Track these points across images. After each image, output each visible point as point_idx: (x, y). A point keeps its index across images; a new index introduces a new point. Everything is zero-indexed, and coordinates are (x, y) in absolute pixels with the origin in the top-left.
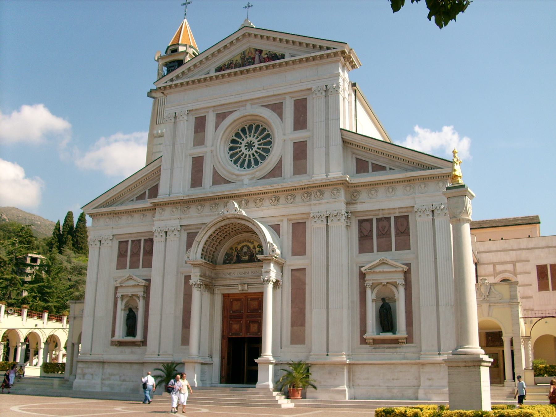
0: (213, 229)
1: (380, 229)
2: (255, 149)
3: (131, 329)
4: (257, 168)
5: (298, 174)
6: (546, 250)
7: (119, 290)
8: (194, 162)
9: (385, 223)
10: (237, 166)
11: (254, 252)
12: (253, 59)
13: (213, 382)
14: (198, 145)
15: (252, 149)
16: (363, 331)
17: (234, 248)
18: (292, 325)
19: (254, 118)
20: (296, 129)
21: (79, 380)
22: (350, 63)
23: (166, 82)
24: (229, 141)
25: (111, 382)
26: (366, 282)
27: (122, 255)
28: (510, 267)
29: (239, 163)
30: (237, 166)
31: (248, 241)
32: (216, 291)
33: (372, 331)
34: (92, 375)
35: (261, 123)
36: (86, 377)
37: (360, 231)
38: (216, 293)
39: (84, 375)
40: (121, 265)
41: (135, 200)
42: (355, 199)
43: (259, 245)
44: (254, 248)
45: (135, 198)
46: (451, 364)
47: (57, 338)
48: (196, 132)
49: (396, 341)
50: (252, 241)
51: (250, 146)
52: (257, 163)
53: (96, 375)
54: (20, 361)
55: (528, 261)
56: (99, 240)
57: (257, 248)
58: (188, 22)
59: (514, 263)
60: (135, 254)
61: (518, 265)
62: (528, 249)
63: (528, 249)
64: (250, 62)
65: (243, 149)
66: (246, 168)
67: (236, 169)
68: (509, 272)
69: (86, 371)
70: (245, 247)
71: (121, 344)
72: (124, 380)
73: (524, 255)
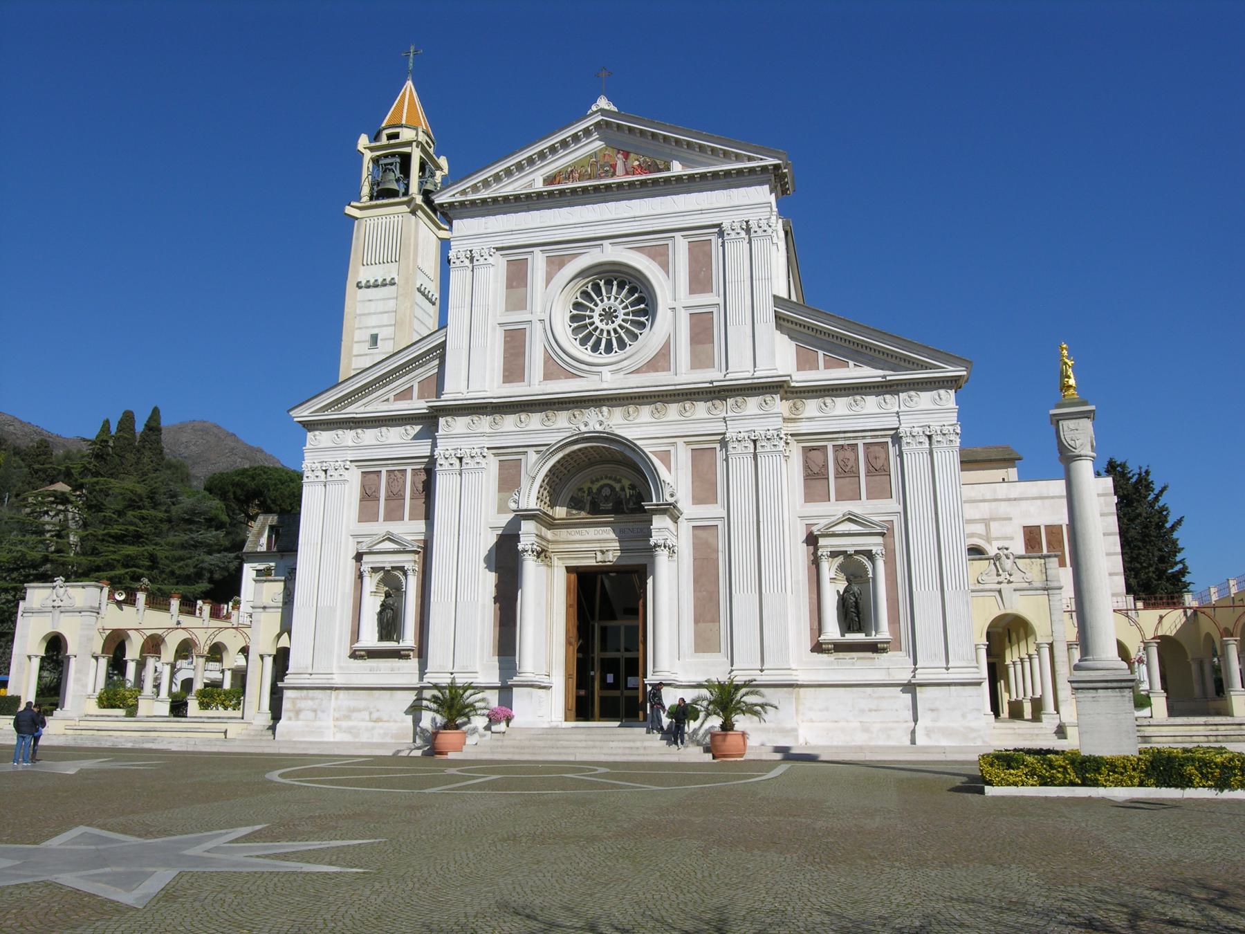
0: (560, 455)
1: (841, 463)
2: (619, 321)
3: (389, 624)
4: (621, 354)
5: (699, 368)
6: (1039, 502)
7: (365, 558)
8: (508, 339)
9: (849, 454)
10: (586, 349)
11: (623, 497)
12: (614, 166)
13: (553, 719)
14: (514, 310)
15: (607, 324)
16: (819, 627)
17: (585, 489)
18: (696, 621)
19: (616, 268)
20: (692, 291)
21: (289, 722)
22: (781, 185)
23: (454, 195)
24: (571, 307)
25: (351, 723)
26: (820, 550)
27: (368, 496)
28: (979, 529)
29: (590, 343)
30: (586, 349)
31: (610, 478)
32: (556, 562)
33: (370, 637)
34: (315, 711)
35: (629, 277)
36: (302, 716)
37: (807, 466)
38: (556, 564)
39: (298, 712)
40: (367, 514)
41: (392, 398)
42: (799, 413)
43: (631, 485)
44: (623, 489)
45: (391, 396)
46: (1075, 685)
47: (62, 644)
48: (510, 286)
49: (874, 648)
50: (618, 477)
51: (609, 315)
52: (622, 345)
53: (323, 712)
54: (232, 685)
55: (1010, 519)
56: (324, 468)
57: (627, 491)
58: (415, 87)
59: (986, 522)
60: (395, 497)
61: (993, 525)
62: (1009, 500)
63: (1009, 500)
64: (607, 171)
65: (596, 319)
66: (603, 352)
67: (585, 354)
68: (980, 536)
69: (302, 704)
70: (605, 488)
71: (373, 654)
72: (378, 720)
73: (1003, 509)
